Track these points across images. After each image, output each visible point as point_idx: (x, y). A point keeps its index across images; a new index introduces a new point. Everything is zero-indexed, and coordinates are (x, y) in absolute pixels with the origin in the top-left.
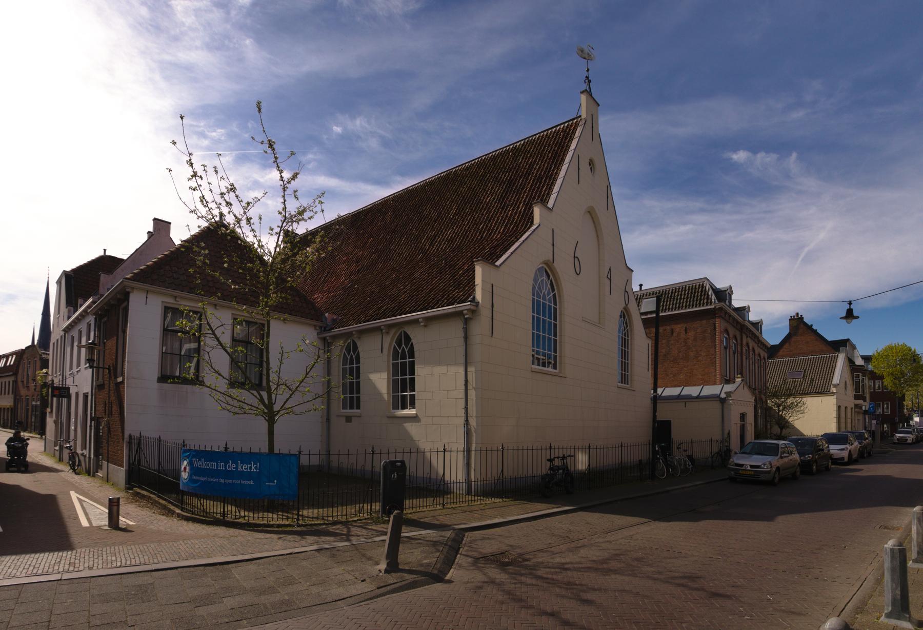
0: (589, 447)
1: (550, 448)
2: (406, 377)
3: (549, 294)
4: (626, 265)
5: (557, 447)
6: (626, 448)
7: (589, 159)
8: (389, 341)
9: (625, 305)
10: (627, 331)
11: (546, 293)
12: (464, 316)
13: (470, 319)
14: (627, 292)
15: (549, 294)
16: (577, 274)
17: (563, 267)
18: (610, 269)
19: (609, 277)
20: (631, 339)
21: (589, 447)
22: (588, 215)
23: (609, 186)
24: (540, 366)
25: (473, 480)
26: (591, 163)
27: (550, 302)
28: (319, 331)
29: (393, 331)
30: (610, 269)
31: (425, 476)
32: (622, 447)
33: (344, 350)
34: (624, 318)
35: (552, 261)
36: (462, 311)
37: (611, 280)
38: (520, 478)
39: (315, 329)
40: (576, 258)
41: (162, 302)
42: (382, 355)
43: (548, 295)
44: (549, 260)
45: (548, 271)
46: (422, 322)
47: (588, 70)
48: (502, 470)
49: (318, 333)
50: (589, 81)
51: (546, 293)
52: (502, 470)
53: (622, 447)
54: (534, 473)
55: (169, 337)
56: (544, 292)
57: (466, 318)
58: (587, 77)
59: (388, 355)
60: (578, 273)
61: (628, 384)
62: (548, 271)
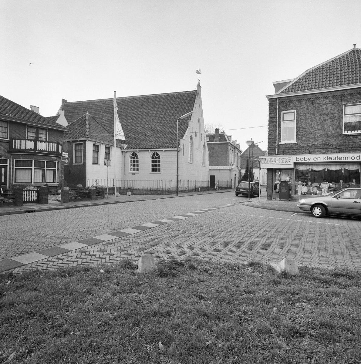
8: (151, 154)
17: (194, 136)
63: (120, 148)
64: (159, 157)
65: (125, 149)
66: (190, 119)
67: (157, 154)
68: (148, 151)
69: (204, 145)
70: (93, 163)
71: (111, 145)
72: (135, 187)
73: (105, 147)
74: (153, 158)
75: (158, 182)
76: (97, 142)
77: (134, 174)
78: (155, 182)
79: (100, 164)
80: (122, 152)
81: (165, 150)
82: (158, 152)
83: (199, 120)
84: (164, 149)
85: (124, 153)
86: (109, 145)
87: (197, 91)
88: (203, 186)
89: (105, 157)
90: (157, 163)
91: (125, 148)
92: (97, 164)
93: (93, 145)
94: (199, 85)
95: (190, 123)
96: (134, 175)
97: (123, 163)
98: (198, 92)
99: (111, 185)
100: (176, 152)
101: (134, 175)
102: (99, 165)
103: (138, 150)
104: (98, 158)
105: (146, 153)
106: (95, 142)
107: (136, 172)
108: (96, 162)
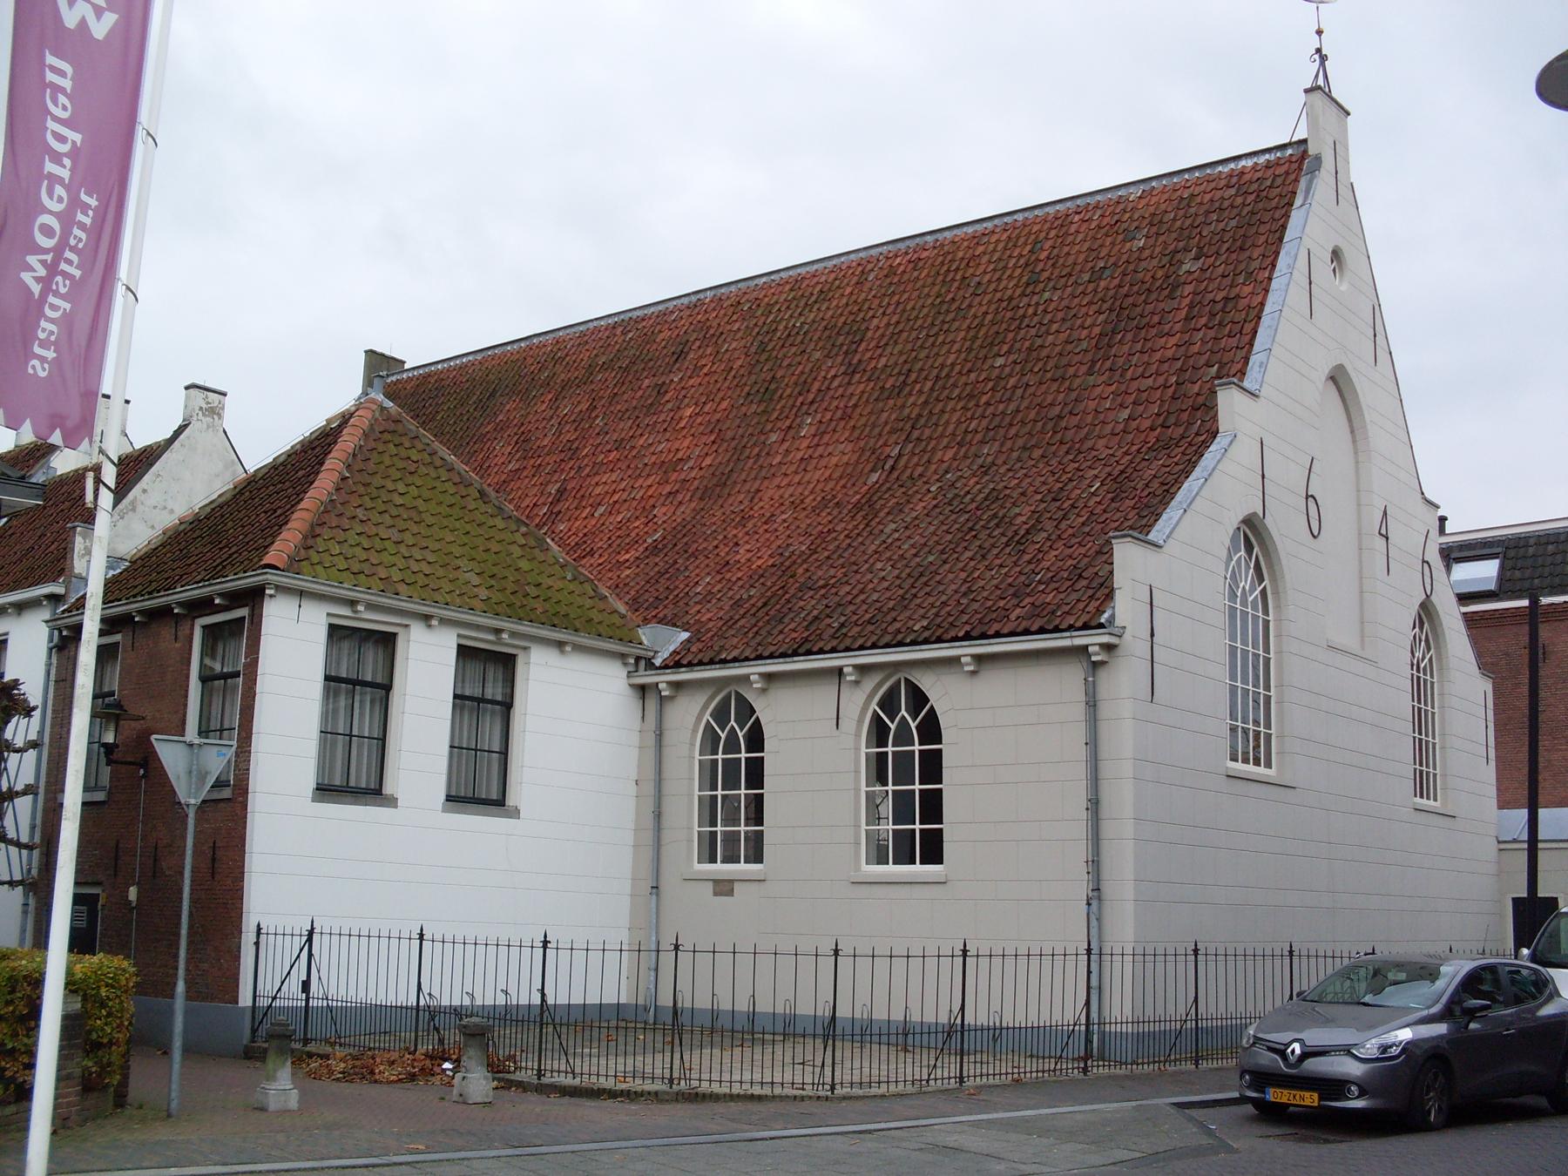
0: (1291, 952)
1: (965, 952)
2: (725, 756)
3: (1252, 590)
4: (1423, 493)
5: (438, 937)
6: (1304, 960)
7: (1331, 250)
8: (859, 703)
9: (1424, 596)
10: (1431, 659)
11: (1247, 588)
12: (1090, 656)
13: (1103, 663)
14: (1428, 563)
15: (1252, 590)
16: (1314, 537)
17: (1285, 527)
18: (1385, 513)
19: (1384, 532)
20: (1278, 620)
21: (1291, 952)
22: (1331, 383)
23: (1377, 308)
24: (1259, 765)
25: (1096, 1021)
26: (1336, 255)
27: (1255, 608)
28: (632, 669)
29: (869, 683)
30: (1385, 513)
31: (820, 1013)
32: (545, 947)
33: (707, 716)
34: (1421, 628)
35: (1261, 516)
36: (1086, 647)
37: (1387, 538)
38: (1032, 1027)
39: (625, 664)
40: (1310, 499)
41: (328, 614)
42: (836, 733)
43: (1252, 592)
44: (1255, 514)
45: (1252, 533)
46: (968, 664)
47: (1319, 32)
48: (963, 1008)
49: (629, 672)
50: (1323, 59)
51: (1247, 588)
52: (963, 1008)
53: (545, 947)
54: (1147, 1015)
55: (488, 718)
56: (1244, 587)
57: (1094, 662)
58: (1319, 51)
59: (858, 735)
60: (1316, 534)
61: (1435, 800)
62: (1252, 533)
63: (622, 657)
64: (931, 730)
65: (665, 667)
66: (1242, 373)
67: (918, 699)
68: (840, 671)
69: (1426, 613)
70: (450, 798)
71: (513, 634)
72: (880, 1014)
73: (460, 647)
74: (879, 733)
75: (806, 964)
76: (371, 607)
77: (724, 887)
78: (765, 962)
79: (399, 795)
80: (643, 690)
81: (979, 659)
82: (928, 683)
83: (1338, 379)
84: (965, 650)
85: (652, 704)
86: (498, 631)
87: (1304, 141)
88: (1208, 1008)
89: (325, 716)
90: (743, 755)
91: (658, 662)
92: (374, 793)
93: (334, 630)
94: (1318, 89)
95: (1229, 402)
96: (730, 893)
97: (649, 788)
98: (1312, 151)
99: (785, 992)
100: (1070, 678)
101: (730, 893)
102: (515, 813)
103: (754, 670)
104: (504, 753)
105: (821, 698)
106: (352, 603)
107: (742, 868)
108: (361, 779)
